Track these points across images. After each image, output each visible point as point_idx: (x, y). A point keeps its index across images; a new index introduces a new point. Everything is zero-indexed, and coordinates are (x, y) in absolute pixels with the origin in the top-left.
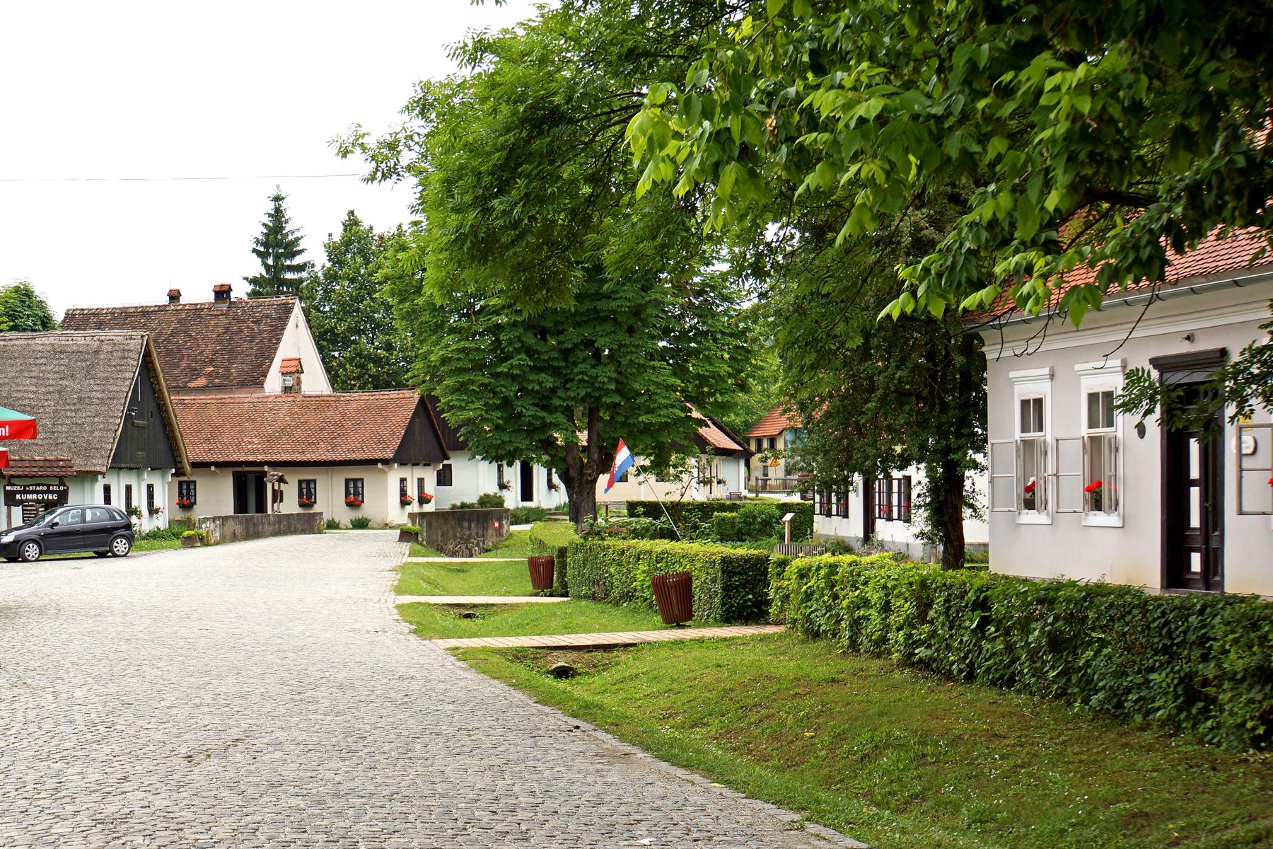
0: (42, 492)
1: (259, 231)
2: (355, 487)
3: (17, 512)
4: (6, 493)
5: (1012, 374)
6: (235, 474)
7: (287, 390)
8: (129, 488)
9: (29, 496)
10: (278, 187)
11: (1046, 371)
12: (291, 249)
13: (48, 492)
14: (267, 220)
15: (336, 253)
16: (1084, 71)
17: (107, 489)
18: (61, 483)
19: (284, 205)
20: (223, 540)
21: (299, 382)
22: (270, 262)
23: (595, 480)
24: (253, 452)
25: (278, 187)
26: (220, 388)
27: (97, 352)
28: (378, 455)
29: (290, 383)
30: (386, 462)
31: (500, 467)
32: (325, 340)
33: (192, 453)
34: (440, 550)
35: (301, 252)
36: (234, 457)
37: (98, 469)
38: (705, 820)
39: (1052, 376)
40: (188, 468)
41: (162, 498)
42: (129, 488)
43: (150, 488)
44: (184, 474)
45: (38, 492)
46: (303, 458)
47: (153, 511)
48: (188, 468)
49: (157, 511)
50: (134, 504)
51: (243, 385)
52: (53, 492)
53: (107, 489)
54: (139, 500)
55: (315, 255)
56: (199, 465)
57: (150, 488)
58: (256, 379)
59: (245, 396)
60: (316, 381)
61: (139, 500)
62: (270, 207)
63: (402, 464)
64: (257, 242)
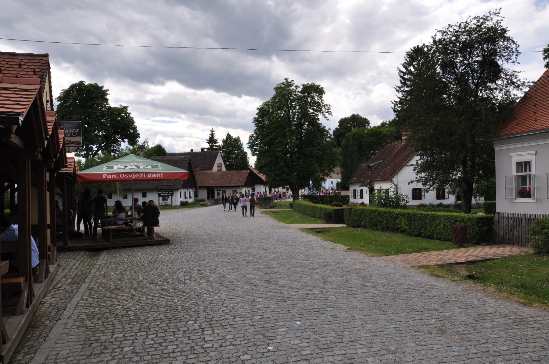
0: (167, 193)
1: (208, 138)
2: (197, 193)
3: (161, 198)
4: (158, 194)
5: (511, 154)
6: (207, 189)
7: (218, 170)
8: (185, 192)
9: (164, 194)
10: (212, 128)
11: (534, 152)
12: (215, 142)
13: (168, 193)
14: (210, 136)
15: (224, 141)
16: (60, 209)
17: (180, 193)
18: (172, 191)
19: (214, 133)
20: (210, 205)
21: (221, 169)
22: (211, 144)
23: (299, 190)
24: (211, 184)
25: (212, 128)
26: (203, 170)
27: (178, 161)
28: (241, 185)
29: (219, 169)
30: (242, 186)
31: (265, 187)
32: (225, 160)
33: (199, 184)
34: (264, 208)
35: (218, 143)
36: (207, 185)
37: (179, 188)
38: (194, 227)
39: (536, 154)
40: (198, 188)
41: (192, 194)
42: (185, 192)
43: (190, 192)
44: (197, 189)
45: (166, 193)
46: (223, 185)
47: (190, 198)
48: (198, 188)
49: (191, 198)
50: (186, 196)
51: (208, 169)
52: (170, 193)
53: (180, 193)
54: (187, 195)
55: (220, 143)
56: (200, 187)
57: (190, 192)
58: (211, 168)
59: (208, 172)
60: (224, 169)
61: (187, 195)
62: (211, 133)
63: (245, 187)
64: (208, 140)
